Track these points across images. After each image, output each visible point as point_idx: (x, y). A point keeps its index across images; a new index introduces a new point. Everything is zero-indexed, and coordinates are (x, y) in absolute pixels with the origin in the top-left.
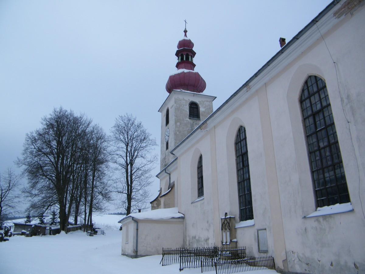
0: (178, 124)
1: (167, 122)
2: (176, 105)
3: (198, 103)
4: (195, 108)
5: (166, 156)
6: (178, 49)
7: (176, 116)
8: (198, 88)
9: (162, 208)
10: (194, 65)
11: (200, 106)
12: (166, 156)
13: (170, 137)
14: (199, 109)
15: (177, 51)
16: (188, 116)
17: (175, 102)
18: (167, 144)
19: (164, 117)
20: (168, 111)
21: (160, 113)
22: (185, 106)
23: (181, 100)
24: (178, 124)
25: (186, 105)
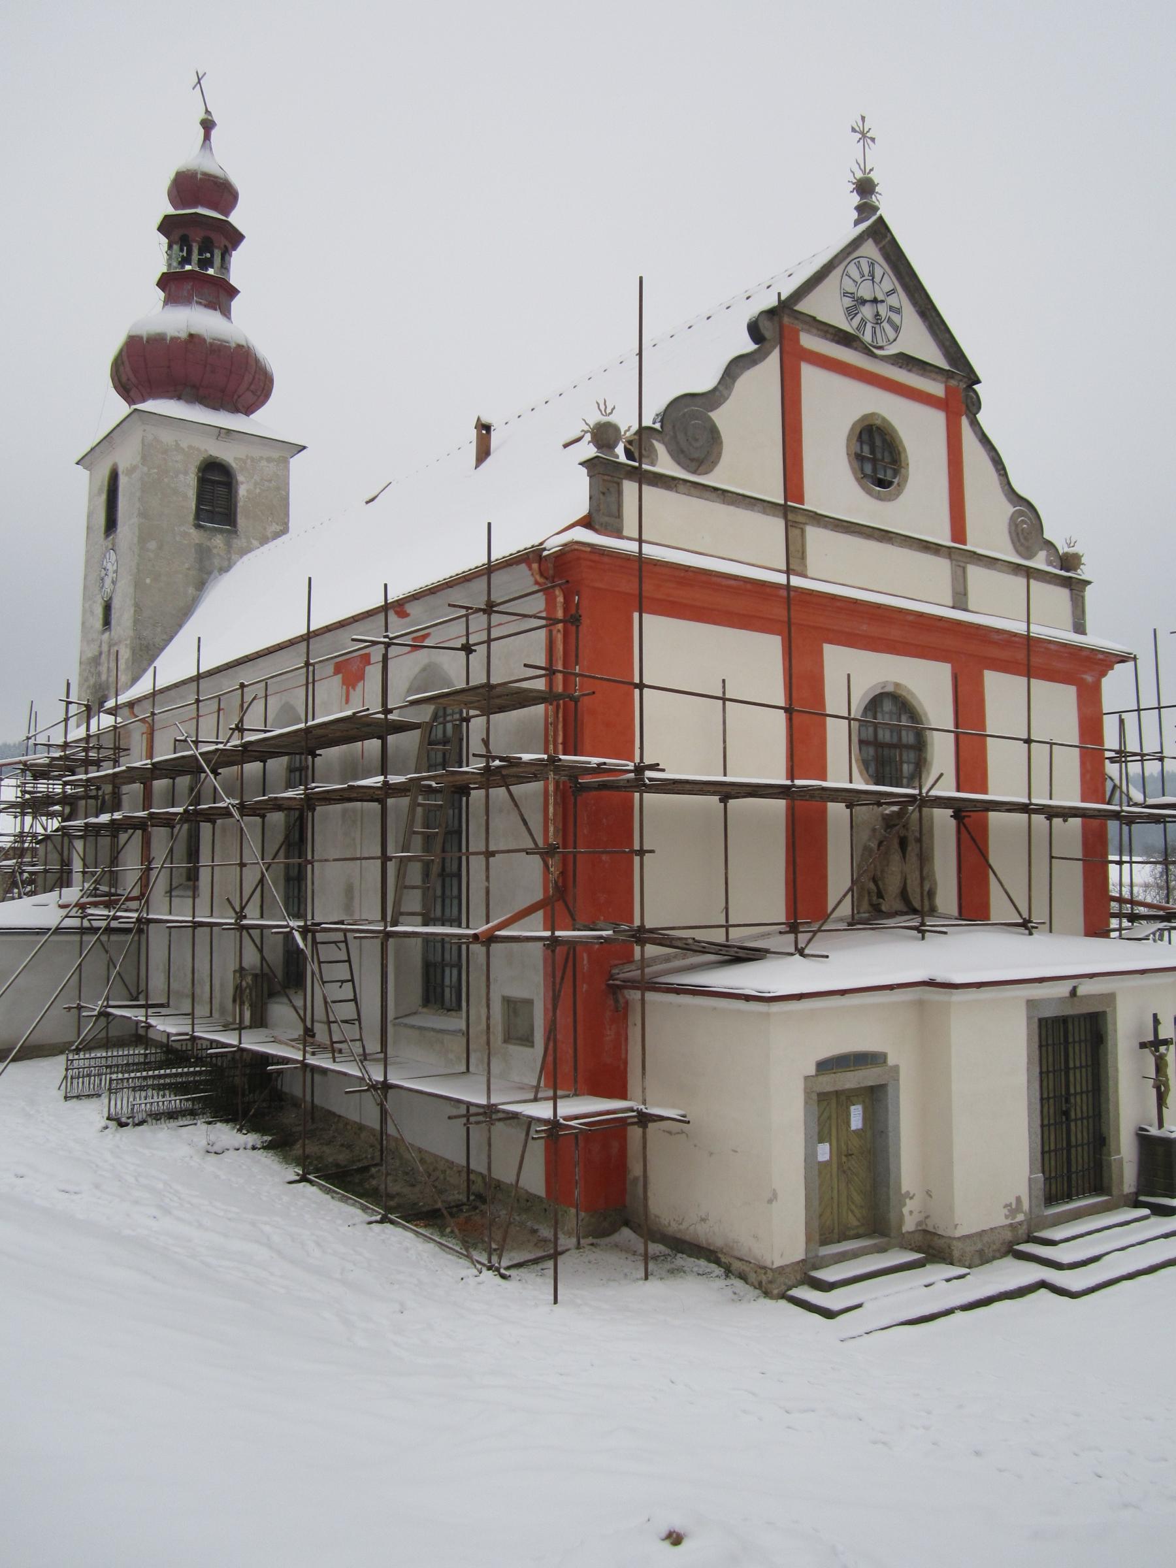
0: (152, 545)
1: (111, 524)
2: (145, 469)
3: (234, 465)
4: (219, 483)
5: (101, 653)
6: (171, 211)
7: (143, 514)
8: (239, 397)
9: (1069, 932)
10: (232, 292)
11: (240, 478)
12: (101, 653)
13: (119, 584)
14: (236, 492)
15: (164, 274)
16: (191, 517)
17: (144, 458)
18: (107, 608)
19: (99, 494)
20: (114, 477)
21: (83, 474)
22: (181, 477)
23: (165, 452)
24: (152, 545)
25: (186, 473)
